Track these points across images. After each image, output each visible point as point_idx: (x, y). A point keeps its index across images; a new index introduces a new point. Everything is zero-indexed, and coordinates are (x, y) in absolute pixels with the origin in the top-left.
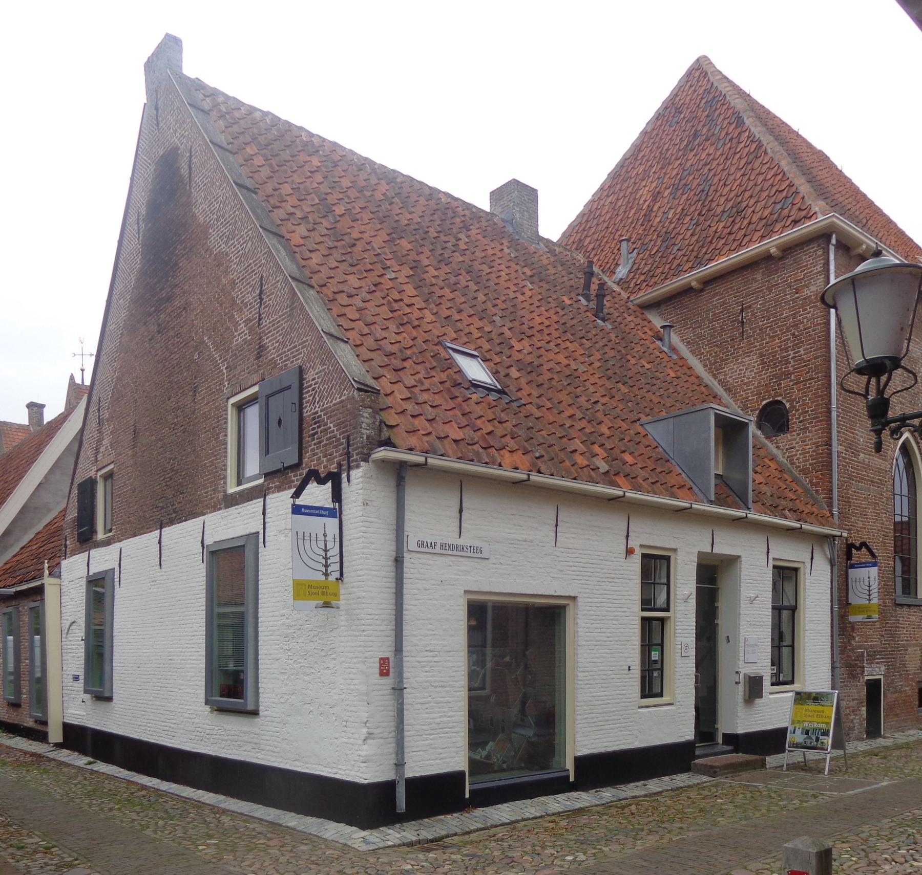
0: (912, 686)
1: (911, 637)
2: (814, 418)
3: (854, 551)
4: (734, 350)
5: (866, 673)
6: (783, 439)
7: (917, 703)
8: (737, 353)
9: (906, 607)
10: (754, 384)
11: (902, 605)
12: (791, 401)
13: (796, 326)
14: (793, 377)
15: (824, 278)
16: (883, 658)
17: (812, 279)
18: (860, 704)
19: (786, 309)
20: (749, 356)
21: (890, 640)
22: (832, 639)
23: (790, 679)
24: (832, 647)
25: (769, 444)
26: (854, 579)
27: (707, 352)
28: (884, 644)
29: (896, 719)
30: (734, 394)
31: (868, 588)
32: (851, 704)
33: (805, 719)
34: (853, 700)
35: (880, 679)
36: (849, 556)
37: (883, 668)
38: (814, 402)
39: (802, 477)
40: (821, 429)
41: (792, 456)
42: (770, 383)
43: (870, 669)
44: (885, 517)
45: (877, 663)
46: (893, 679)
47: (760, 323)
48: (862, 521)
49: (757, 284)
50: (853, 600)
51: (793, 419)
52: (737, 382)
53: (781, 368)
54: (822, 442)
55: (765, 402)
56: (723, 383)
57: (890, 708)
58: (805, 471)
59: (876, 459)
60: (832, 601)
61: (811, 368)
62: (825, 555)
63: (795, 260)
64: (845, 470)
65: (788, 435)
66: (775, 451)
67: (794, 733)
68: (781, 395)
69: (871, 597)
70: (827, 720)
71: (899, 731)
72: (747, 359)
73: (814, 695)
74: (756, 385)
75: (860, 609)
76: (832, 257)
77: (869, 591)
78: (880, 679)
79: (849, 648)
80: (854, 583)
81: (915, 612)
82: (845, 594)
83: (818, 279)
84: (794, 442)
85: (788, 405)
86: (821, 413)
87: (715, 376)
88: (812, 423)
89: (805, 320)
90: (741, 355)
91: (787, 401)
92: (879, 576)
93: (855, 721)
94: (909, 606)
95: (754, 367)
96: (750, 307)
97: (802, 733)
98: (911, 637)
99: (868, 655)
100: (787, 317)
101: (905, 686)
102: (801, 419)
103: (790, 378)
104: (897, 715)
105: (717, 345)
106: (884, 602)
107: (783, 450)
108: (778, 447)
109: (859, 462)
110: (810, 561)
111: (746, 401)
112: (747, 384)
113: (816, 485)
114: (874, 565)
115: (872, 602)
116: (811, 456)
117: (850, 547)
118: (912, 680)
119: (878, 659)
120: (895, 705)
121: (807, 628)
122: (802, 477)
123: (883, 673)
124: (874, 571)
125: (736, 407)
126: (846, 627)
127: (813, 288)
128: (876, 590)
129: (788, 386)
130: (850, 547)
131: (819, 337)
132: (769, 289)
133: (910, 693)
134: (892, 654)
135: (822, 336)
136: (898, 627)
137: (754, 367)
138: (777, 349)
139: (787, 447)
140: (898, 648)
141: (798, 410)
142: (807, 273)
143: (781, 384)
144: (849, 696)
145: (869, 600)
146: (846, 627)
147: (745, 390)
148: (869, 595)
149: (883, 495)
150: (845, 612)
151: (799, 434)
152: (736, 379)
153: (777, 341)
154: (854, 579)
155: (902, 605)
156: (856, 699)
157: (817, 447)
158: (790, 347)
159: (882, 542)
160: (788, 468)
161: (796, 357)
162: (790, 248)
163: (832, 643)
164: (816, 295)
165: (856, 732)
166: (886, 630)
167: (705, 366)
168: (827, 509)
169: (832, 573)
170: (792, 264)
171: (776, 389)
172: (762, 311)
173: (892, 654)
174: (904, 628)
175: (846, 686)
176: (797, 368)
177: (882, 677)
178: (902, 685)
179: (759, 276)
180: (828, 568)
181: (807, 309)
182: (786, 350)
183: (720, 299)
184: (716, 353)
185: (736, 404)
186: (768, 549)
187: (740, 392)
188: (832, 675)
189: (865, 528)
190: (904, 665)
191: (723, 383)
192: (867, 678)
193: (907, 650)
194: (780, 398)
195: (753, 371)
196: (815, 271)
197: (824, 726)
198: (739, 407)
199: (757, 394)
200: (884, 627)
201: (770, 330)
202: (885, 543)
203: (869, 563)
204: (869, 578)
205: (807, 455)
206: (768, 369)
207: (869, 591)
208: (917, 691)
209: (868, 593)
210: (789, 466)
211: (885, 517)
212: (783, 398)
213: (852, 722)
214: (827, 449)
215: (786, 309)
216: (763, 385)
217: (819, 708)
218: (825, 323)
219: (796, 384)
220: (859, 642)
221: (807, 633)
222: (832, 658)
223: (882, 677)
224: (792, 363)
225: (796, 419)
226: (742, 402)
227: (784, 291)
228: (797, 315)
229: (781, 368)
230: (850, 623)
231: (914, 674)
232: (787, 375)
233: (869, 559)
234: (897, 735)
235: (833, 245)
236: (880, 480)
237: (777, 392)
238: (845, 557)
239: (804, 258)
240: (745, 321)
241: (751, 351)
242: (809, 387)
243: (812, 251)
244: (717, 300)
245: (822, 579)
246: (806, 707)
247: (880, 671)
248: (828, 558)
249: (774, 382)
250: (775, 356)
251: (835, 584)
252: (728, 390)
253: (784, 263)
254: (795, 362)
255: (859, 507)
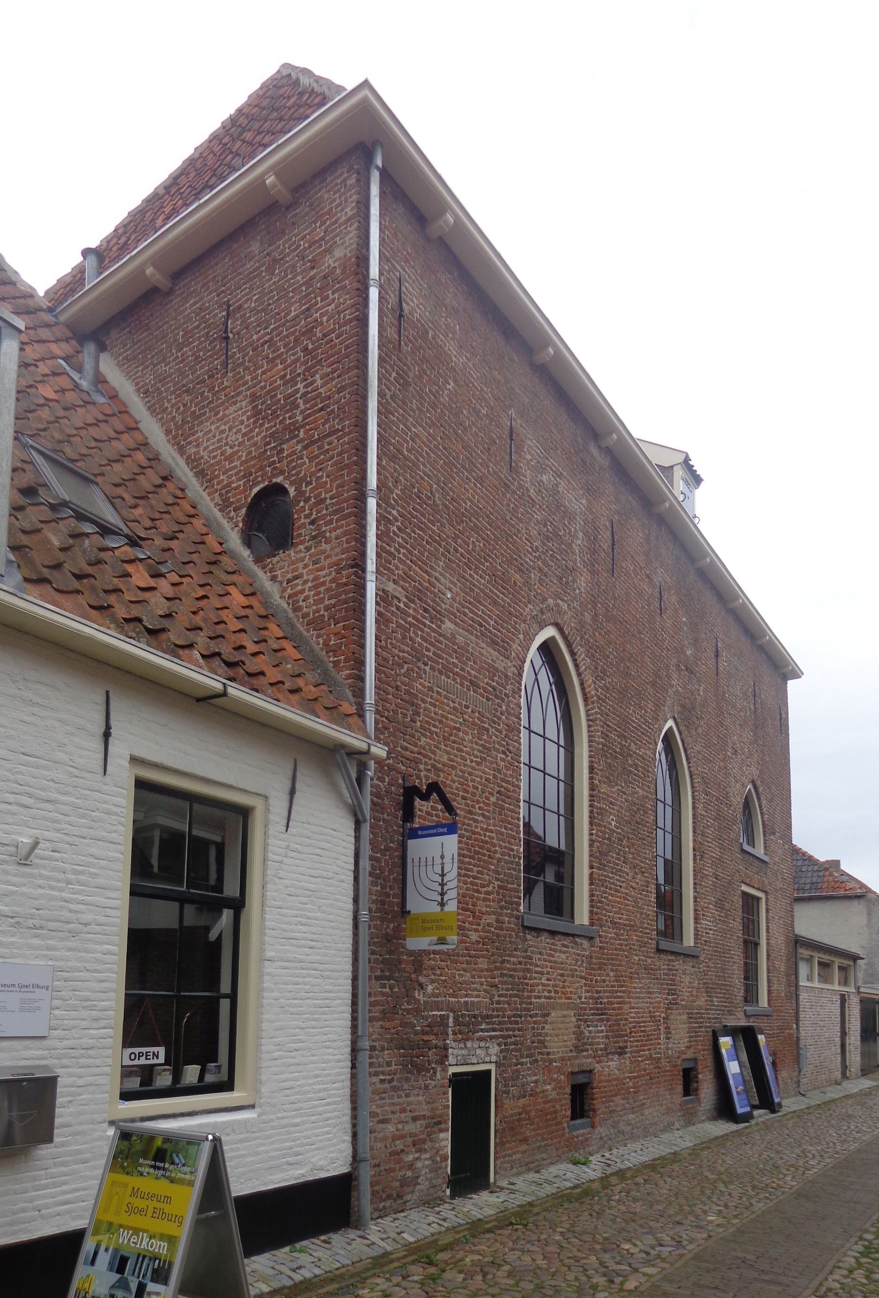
0: (558, 1081)
1: (556, 992)
2: (336, 512)
3: (417, 802)
4: (214, 395)
5: (452, 1060)
6: (283, 561)
7: (569, 1113)
8: (218, 399)
9: (546, 934)
10: (239, 458)
11: (538, 931)
12: (298, 483)
13: (309, 332)
14: (302, 434)
15: (358, 229)
16: (494, 1030)
17: (337, 235)
18: (437, 1123)
19: (296, 302)
20: (235, 403)
21: (511, 996)
22: (355, 987)
23: (225, 1077)
24: (354, 1004)
25: (260, 573)
26: (416, 860)
27: (172, 407)
28: (498, 1003)
29: (523, 1147)
30: (210, 481)
31: (439, 879)
32: (411, 1127)
33: (124, 1219)
34: (415, 1119)
35: (488, 1072)
36: (408, 813)
37: (494, 1049)
38: (336, 478)
39: (310, 635)
40: (345, 533)
41: (296, 594)
42: (266, 451)
43: (464, 1052)
44: (502, 760)
45: (481, 1039)
46: (517, 1071)
47: (255, 337)
48: (448, 753)
49: (252, 263)
50: (416, 904)
51: (299, 518)
52: (215, 457)
53: (284, 419)
54: (348, 559)
55: (255, 490)
56: (193, 461)
57: (511, 1128)
58: (316, 623)
59: (484, 645)
60: (356, 900)
61: (333, 411)
62: (340, 795)
63: (311, 205)
64: (404, 637)
65: (292, 552)
66: (268, 585)
67: (93, 1263)
68: (282, 472)
69: (446, 898)
70: (170, 1229)
71: (529, 1170)
72: (232, 409)
73: (159, 1142)
74: (243, 459)
75: (426, 924)
76: (375, 190)
77: (442, 885)
78: (488, 1072)
79: (405, 1006)
80: (416, 869)
81: (564, 946)
82: (397, 891)
83: (349, 232)
84: (300, 565)
85: (292, 491)
86: (346, 500)
87: (181, 450)
88: (330, 522)
89: (325, 319)
90: (223, 403)
91: (291, 484)
92: (459, 855)
93: (419, 1164)
94: (553, 933)
95: (242, 422)
96: (240, 307)
97: (111, 1269)
98: (556, 992)
99: (457, 1022)
100: (297, 316)
101: (544, 1082)
102: (314, 516)
103: (297, 436)
104: (525, 1140)
105: (187, 391)
106: (498, 921)
107: (281, 583)
108: (273, 579)
109: (441, 635)
110: (286, 797)
111: (227, 492)
112: (229, 459)
113: (335, 651)
114: (451, 829)
115: (446, 908)
116: (328, 590)
117: (411, 793)
118: (559, 1070)
119: (482, 1031)
120: (519, 1120)
121: (269, 954)
122: (310, 635)
123: (494, 1059)
124: (451, 843)
125: (212, 505)
126: (400, 962)
127: (338, 253)
128: (454, 884)
129: (294, 453)
130: (411, 793)
131: (347, 347)
132: (271, 270)
133: (553, 1095)
134: (517, 1023)
135: (352, 344)
136: (529, 971)
137: (242, 422)
138: (279, 382)
139: (289, 576)
140: (528, 1010)
141: (309, 498)
142: (330, 226)
143: (282, 450)
144: (403, 1111)
145: (442, 904)
146: (400, 962)
147: (227, 471)
148: (442, 894)
149: (499, 719)
150: (397, 929)
151: (308, 549)
152: (213, 451)
153: (280, 367)
154: (416, 860)
155: (538, 931)
156: (424, 1117)
157: (338, 572)
158: (299, 375)
159: (494, 804)
160: (288, 619)
161: (308, 393)
162: (303, 185)
163: (355, 996)
164: (344, 267)
165: (423, 1185)
166: (502, 975)
167: (168, 432)
168: (352, 699)
169: (357, 838)
170: (307, 214)
171: (274, 462)
172: (258, 312)
173: (517, 1023)
174: (542, 973)
175: (394, 1089)
176: (309, 415)
177: (492, 1067)
178: (536, 1082)
179: (255, 247)
180: (347, 826)
181: (327, 297)
182: (293, 381)
183: (195, 303)
184: (185, 405)
185: (212, 500)
186: (108, 727)
187: (218, 476)
188: (353, 1067)
189: (454, 768)
190: (542, 1042)
191: (193, 461)
192: (452, 1070)
193: (548, 1015)
194: (279, 480)
195: (239, 431)
196: (344, 218)
197: (160, 1248)
198: (216, 504)
199: (244, 477)
200: (497, 968)
201: (269, 348)
202: (502, 808)
203: (443, 826)
204: (442, 857)
205: (322, 589)
206: (262, 425)
207: (442, 885)
208: (568, 1090)
209: (439, 889)
210: (291, 614)
211: (502, 760)
212: (285, 478)
213: (411, 1166)
214: (356, 574)
215: (296, 302)
216: (255, 458)
217: (162, 1187)
218: (357, 319)
219: (305, 447)
220: (433, 995)
221: (269, 968)
222: (354, 1027)
223: (492, 1067)
224: (302, 407)
225: (306, 517)
226: (221, 495)
227: (294, 267)
228: (312, 311)
229: (284, 419)
230: (411, 953)
231: (563, 1059)
232: (292, 429)
233: (445, 817)
234: (520, 1182)
235: (377, 167)
236: (494, 688)
237: (275, 468)
238: (400, 814)
239: (326, 196)
240: (231, 335)
241: (239, 394)
242: (328, 451)
243: (339, 181)
244: (191, 306)
245: (326, 846)
246: (134, 1181)
247: (488, 1055)
248: (346, 804)
249: (271, 449)
250: (275, 395)
251: (365, 864)
252: (200, 474)
253: (295, 215)
254: (305, 403)
255: (440, 722)
